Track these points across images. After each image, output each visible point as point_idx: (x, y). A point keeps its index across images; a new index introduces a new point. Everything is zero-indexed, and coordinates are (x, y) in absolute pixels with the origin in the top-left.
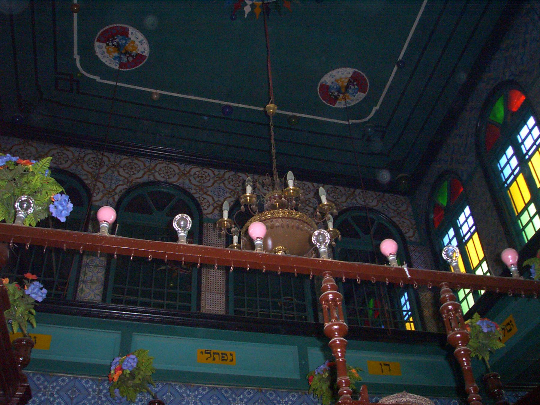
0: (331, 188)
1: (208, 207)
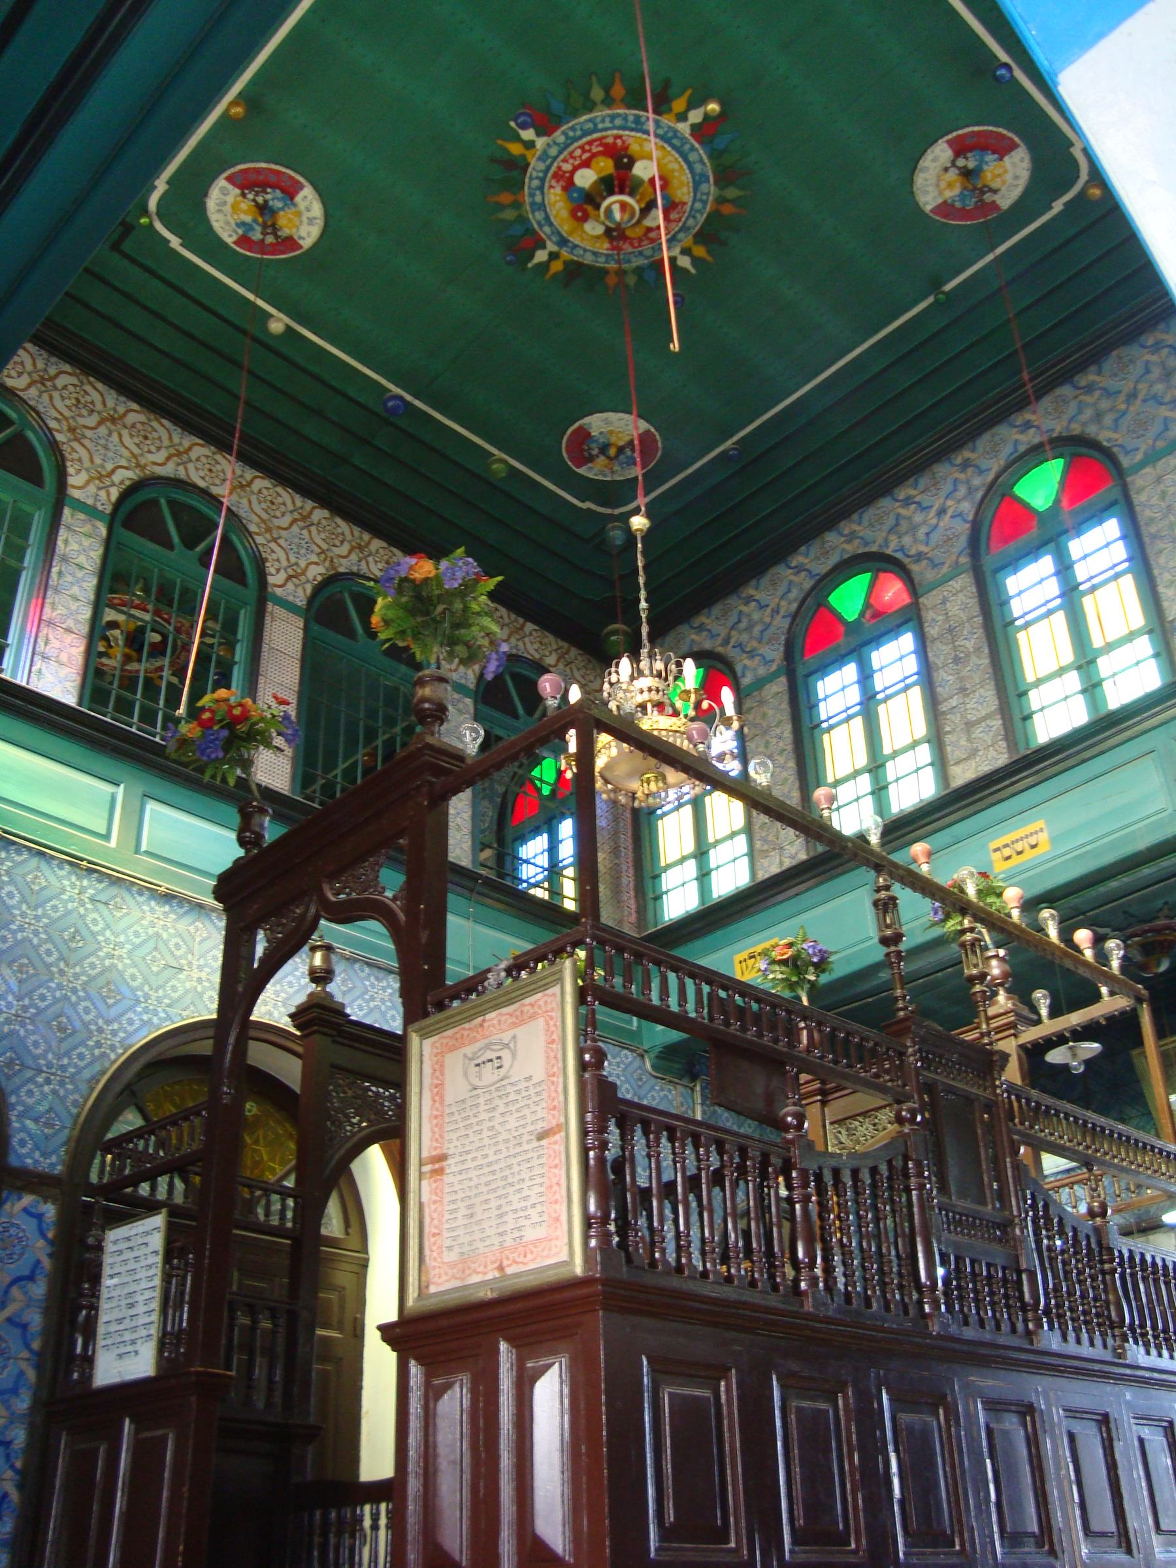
0: (75, 386)
1: (278, 571)
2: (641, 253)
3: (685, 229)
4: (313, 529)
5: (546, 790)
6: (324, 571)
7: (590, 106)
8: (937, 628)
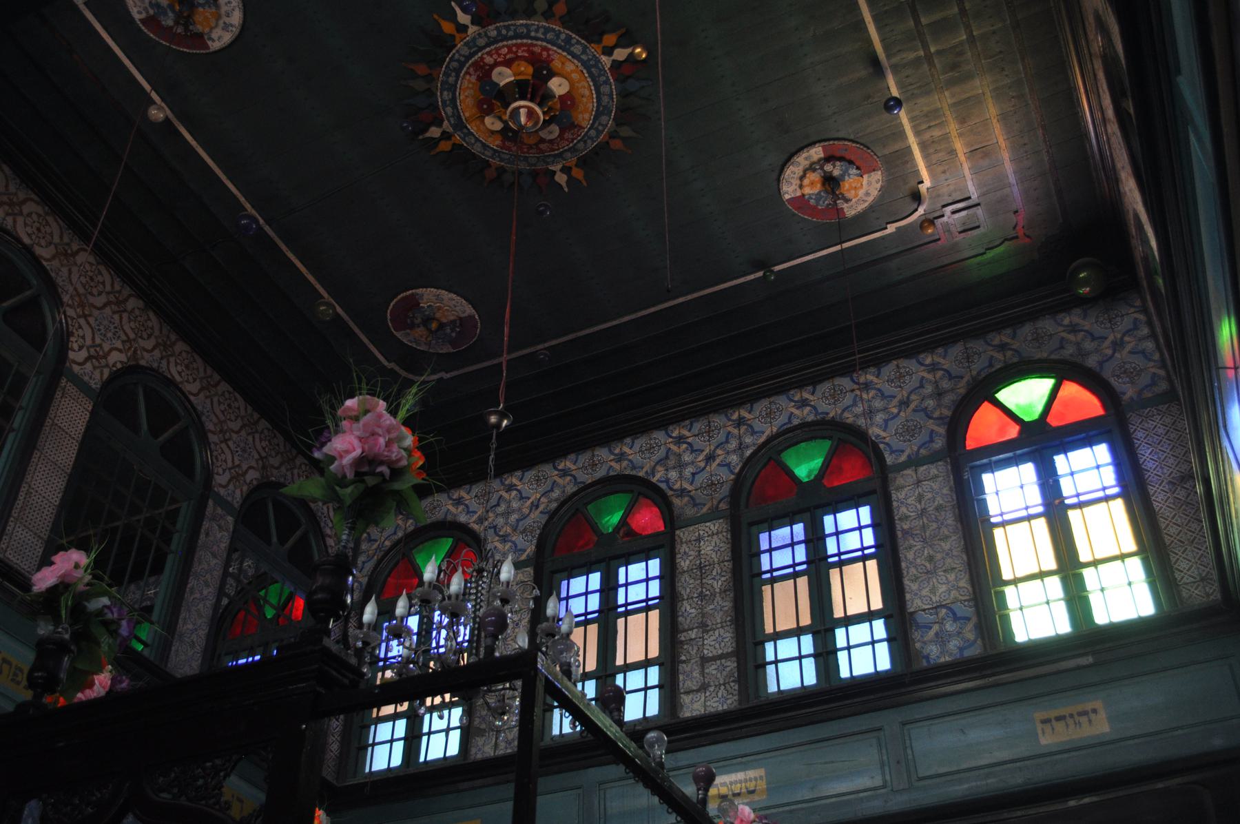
1: (81, 348)
2: (526, 159)
3: (573, 150)
4: (125, 315)
5: (270, 613)
6: (125, 360)
7: (530, 13)
8: (688, 562)
